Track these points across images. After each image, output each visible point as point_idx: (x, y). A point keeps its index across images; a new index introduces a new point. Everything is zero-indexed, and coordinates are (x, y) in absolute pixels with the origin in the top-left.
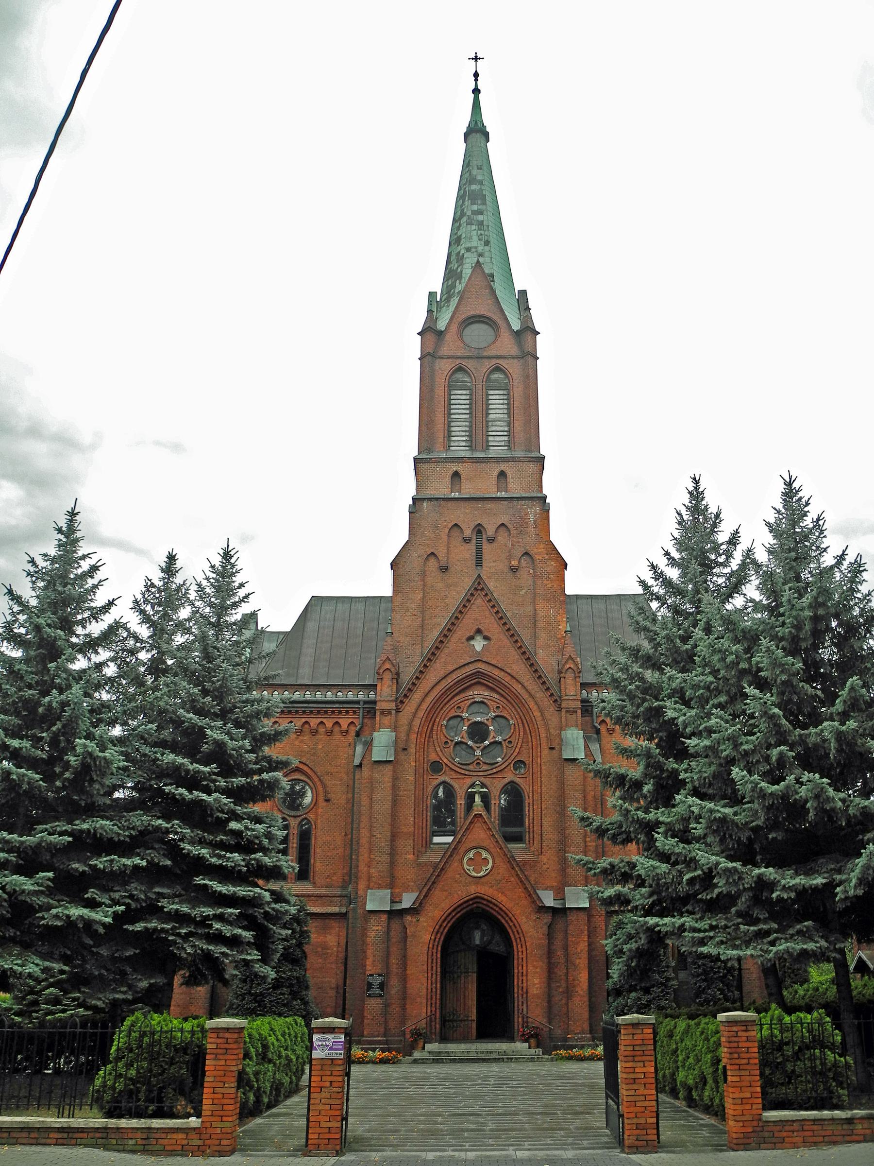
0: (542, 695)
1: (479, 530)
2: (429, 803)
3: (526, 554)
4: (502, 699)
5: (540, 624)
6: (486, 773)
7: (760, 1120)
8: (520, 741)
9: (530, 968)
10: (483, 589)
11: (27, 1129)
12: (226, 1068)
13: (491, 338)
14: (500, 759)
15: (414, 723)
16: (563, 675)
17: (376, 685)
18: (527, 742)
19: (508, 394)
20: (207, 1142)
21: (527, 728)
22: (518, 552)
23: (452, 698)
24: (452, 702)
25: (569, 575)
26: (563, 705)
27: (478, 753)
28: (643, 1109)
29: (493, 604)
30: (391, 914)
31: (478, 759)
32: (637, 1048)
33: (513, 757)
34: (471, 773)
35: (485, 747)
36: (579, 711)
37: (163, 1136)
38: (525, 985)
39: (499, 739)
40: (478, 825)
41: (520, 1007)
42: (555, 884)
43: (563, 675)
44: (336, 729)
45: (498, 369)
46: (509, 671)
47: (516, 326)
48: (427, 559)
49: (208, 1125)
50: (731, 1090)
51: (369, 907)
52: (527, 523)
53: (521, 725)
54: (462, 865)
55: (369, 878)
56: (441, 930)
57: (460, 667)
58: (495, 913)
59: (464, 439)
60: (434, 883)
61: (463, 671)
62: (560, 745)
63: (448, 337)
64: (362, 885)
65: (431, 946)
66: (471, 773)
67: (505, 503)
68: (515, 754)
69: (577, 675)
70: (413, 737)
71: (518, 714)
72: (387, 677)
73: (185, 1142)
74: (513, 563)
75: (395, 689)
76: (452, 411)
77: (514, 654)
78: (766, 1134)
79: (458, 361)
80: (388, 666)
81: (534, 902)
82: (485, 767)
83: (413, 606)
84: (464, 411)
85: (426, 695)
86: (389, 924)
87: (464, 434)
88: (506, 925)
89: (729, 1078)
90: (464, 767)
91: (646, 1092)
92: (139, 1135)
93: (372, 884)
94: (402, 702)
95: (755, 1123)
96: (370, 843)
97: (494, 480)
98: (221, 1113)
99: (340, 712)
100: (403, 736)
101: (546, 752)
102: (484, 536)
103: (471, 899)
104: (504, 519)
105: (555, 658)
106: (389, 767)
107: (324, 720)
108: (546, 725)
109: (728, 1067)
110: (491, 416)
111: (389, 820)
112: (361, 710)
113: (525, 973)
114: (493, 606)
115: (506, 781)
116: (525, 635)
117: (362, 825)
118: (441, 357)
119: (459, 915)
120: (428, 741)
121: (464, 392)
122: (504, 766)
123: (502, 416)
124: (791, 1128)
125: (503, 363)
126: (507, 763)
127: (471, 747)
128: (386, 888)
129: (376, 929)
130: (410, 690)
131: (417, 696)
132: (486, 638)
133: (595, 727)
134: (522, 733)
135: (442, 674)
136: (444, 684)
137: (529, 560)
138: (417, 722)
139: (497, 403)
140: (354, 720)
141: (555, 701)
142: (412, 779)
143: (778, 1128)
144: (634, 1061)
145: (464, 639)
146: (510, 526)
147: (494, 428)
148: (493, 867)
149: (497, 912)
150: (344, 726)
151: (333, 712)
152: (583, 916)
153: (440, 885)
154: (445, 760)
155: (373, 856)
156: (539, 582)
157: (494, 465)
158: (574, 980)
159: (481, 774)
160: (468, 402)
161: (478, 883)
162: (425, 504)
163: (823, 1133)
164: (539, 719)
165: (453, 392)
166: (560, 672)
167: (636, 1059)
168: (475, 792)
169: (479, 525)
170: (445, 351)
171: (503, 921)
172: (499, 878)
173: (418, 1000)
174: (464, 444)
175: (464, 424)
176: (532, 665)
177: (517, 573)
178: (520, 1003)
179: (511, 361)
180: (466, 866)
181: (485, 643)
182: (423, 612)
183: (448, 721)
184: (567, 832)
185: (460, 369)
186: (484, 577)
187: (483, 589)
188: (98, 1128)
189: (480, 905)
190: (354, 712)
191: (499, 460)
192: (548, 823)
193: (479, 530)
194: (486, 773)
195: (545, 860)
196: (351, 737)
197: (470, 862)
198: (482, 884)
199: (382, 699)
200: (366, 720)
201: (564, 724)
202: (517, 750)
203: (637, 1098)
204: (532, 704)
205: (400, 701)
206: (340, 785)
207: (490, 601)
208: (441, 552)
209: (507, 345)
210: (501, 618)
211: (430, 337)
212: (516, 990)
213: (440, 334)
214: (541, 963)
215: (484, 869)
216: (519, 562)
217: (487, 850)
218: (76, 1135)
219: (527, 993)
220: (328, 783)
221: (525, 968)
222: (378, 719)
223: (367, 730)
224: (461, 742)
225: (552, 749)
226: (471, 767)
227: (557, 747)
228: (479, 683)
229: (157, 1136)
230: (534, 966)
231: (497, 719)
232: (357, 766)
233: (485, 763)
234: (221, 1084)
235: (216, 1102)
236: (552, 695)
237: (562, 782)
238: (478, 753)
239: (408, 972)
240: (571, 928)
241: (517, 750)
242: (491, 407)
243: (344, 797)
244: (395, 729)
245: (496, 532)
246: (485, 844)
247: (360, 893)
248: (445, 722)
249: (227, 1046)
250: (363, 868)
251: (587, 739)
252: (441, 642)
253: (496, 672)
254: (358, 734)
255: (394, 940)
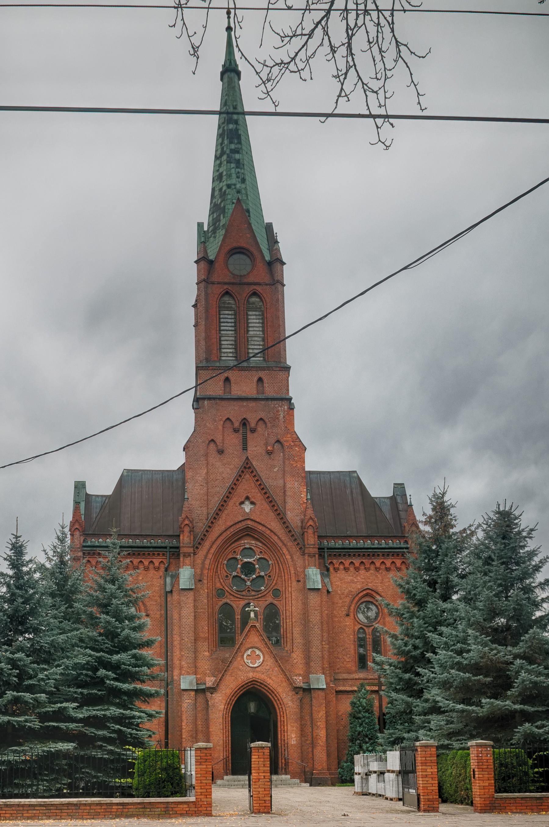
0: (292, 544)
1: (244, 423)
2: (217, 617)
3: (278, 441)
4: (264, 546)
5: (288, 493)
6: (254, 597)
7: (493, 797)
8: (276, 576)
9: (289, 727)
10: (250, 468)
11: (77, 806)
12: (207, 770)
13: (249, 268)
14: (263, 588)
15: (206, 562)
16: (306, 530)
17: (179, 536)
18: (281, 577)
19: (263, 315)
20: (200, 809)
21: (281, 567)
22: (272, 440)
23: (230, 546)
24: (230, 548)
25: (308, 456)
26: (306, 551)
27: (248, 583)
28: (431, 791)
29: (258, 479)
30: (197, 691)
31: (249, 588)
32: (427, 759)
33: (272, 586)
34: (244, 597)
35: (253, 579)
36: (317, 556)
37: (175, 806)
38: (286, 738)
39: (262, 574)
40: (253, 632)
41: (283, 752)
42: (302, 673)
43: (306, 530)
44: (151, 566)
45: (255, 294)
46: (269, 527)
47: (268, 258)
48: (209, 444)
49: (199, 800)
50: (477, 782)
51: (183, 687)
52: (278, 418)
53: (277, 565)
54: (243, 659)
55: (181, 668)
56: (231, 702)
57: (235, 524)
58: (265, 691)
59: (231, 351)
60: (226, 671)
61: (238, 526)
62: (304, 578)
63: (217, 265)
64: (176, 672)
65: (225, 713)
66: (244, 597)
67: (263, 402)
68: (273, 584)
69: (315, 530)
70: (206, 572)
71: (275, 556)
72: (187, 529)
73: (187, 809)
74: (269, 448)
75: (192, 539)
76: (222, 328)
77: (272, 515)
78: (497, 805)
79: (226, 287)
80: (187, 522)
81: (291, 684)
82: (253, 593)
83: (200, 479)
84: (230, 328)
85: (213, 544)
86: (196, 699)
87: (231, 347)
88: (273, 699)
89: (477, 776)
90: (240, 593)
91: (433, 782)
92: (162, 806)
93: (183, 672)
94: (197, 548)
95: (491, 799)
96: (180, 644)
97: (254, 385)
98: (206, 794)
99: (154, 554)
100: (199, 571)
101: (294, 583)
102: (248, 428)
103: (250, 682)
104: (262, 415)
105: (298, 518)
106: (191, 593)
107: (143, 560)
108: (295, 565)
109: (476, 770)
110: (251, 333)
111: (193, 629)
112: (168, 553)
113: (286, 730)
114: (257, 480)
115: (268, 603)
116: (278, 499)
117: (175, 632)
118: (213, 283)
119: (242, 692)
120: (215, 575)
121: (230, 313)
122: (266, 593)
123: (258, 333)
124: (510, 802)
125: (259, 289)
126: (268, 591)
127: (243, 580)
128: (192, 674)
129: (187, 702)
130: (202, 539)
131: (207, 544)
132: (252, 503)
133: (326, 567)
134: (277, 570)
135: (223, 528)
136: (225, 535)
137: (280, 446)
138: (207, 562)
139: (254, 320)
140: (163, 560)
141: (301, 548)
142: (206, 601)
143: (503, 802)
144: (426, 766)
145: (237, 504)
146: (267, 421)
147: (253, 343)
148: (263, 661)
149: (267, 690)
150: (157, 564)
151: (149, 554)
152: (322, 694)
153: (229, 673)
154: (227, 588)
155: (183, 653)
156: (287, 462)
157: (254, 372)
158: (317, 736)
159: (251, 598)
160: (233, 321)
161: (254, 672)
162: (206, 402)
163: (526, 804)
164: (290, 560)
165: (222, 312)
166: (302, 527)
167: (427, 764)
168: (251, 611)
169: (245, 419)
170: (215, 278)
171: (270, 696)
172: (268, 668)
173: (218, 748)
174: (231, 355)
175: (231, 338)
176: (284, 523)
177: (272, 456)
178: (283, 750)
179: (265, 287)
180: (245, 660)
181: (252, 506)
182: (207, 483)
183: (228, 561)
184: (310, 638)
185: (227, 293)
186: (249, 458)
187: (250, 468)
188: (139, 803)
189: (256, 686)
190: (163, 555)
191: (258, 368)
192: (297, 631)
193: (244, 423)
194: (254, 597)
195: (295, 657)
196: (161, 572)
197: (248, 658)
198: (257, 672)
199: (184, 545)
200: (171, 560)
201: (307, 564)
202: (275, 582)
203: (428, 785)
204: (285, 550)
205: (197, 547)
206: (155, 605)
207: (255, 476)
208: (219, 440)
209: (260, 274)
210: (263, 488)
211: (203, 264)
212: (280, 742)
213: (211, 263)
214: (296, 724)
215: (258, 662)
216: (273, 447)
217: (260, 650)
218: (127, 807)
219: (287, 744)
220: (148, 604)
221: (286, 727)
222: (181, 559)
223: (172, 568)
224: (237, 576)
225: (299, 581)
226: (244, 593)
227: (302, 580)
228: (248, 535)
229: (172, 806)
230: (291, 726)
231: (261, 560)
232: (169, 592)
233: (252, 590)
234: (205, 778)
235: (202, 787)
236: (298, 544)
237: (305, 604)
238: (248, 583)
239: (211, 730)
240: (314, 701)
241: (275, 582)
242: (250, 325)
243: (159, 613)
244: (193, 566)
245: (256, 425)
246: (258, 645)
247: (175, 678)
248: (226, 562)
249: (206, 758)
250: (176, 662)
251: (322, 575)
252: (222, 505)
253: (261, 527)
254: (166, 570)
255: (199, 709)
